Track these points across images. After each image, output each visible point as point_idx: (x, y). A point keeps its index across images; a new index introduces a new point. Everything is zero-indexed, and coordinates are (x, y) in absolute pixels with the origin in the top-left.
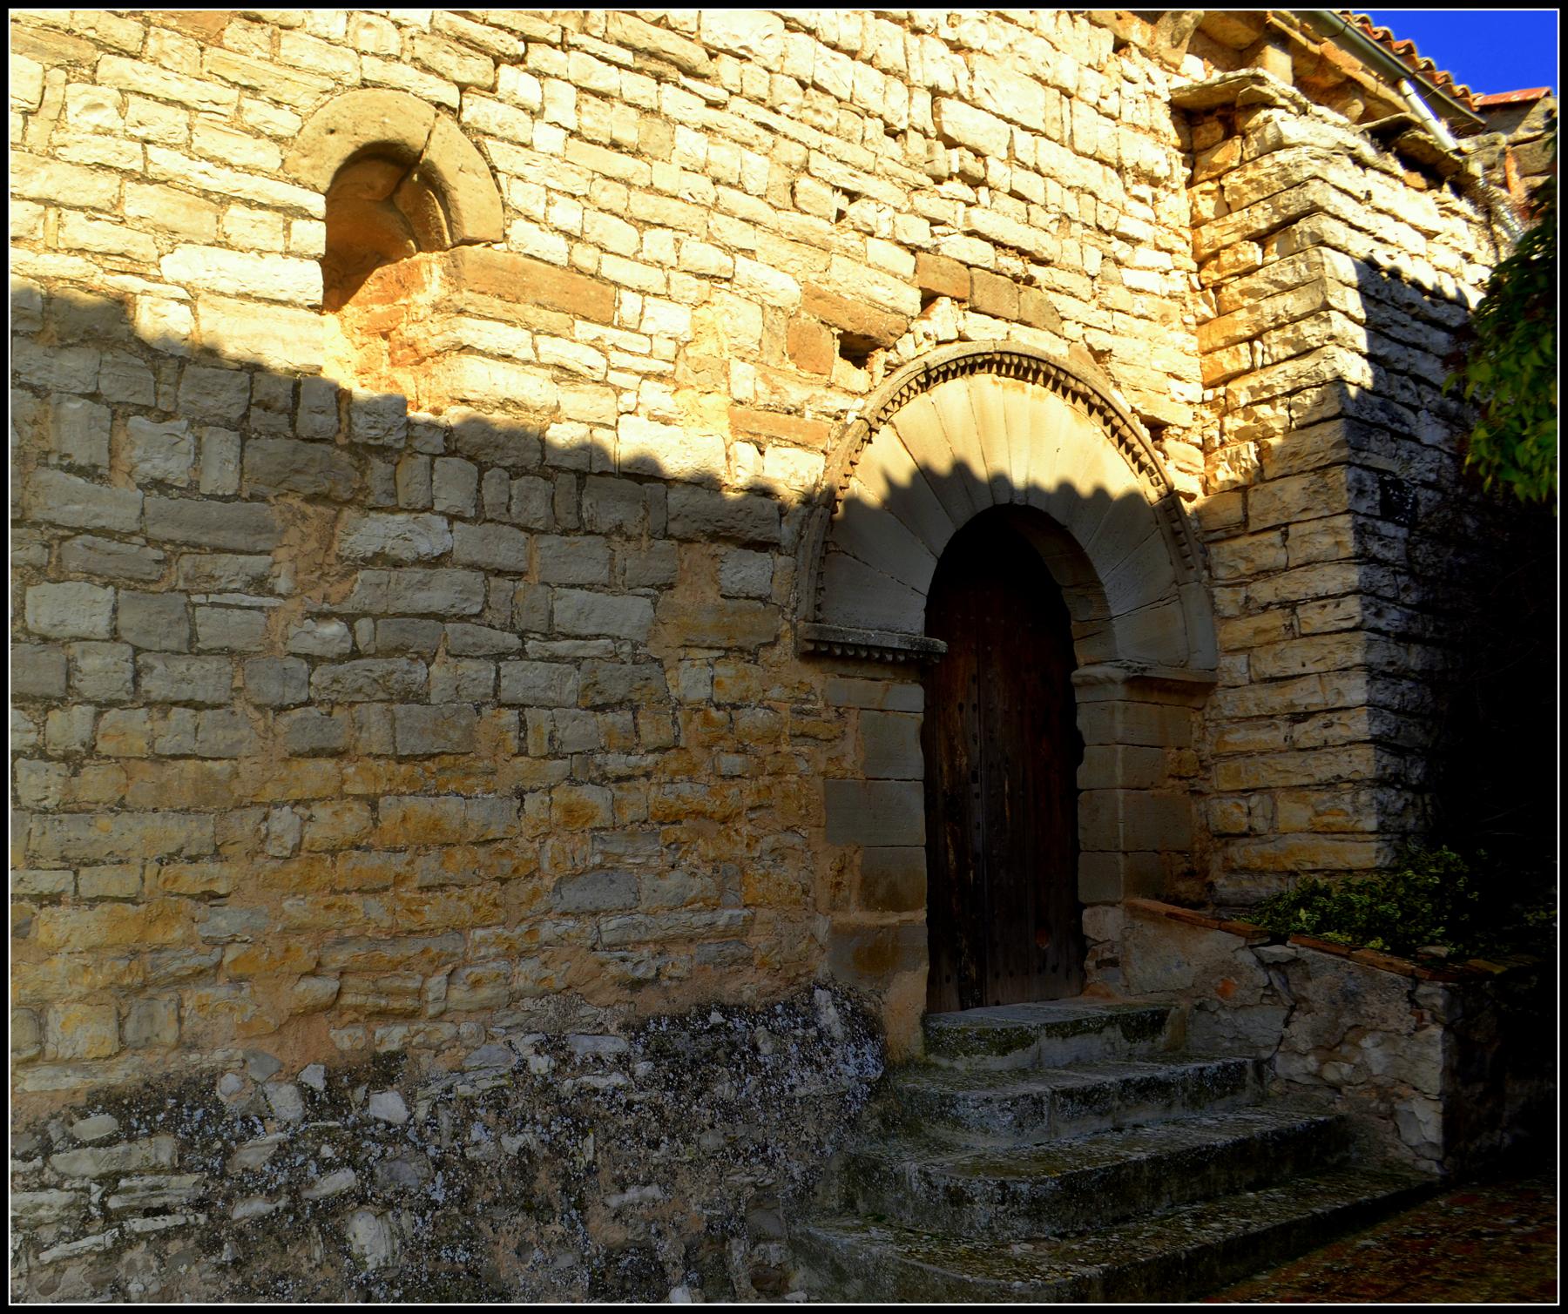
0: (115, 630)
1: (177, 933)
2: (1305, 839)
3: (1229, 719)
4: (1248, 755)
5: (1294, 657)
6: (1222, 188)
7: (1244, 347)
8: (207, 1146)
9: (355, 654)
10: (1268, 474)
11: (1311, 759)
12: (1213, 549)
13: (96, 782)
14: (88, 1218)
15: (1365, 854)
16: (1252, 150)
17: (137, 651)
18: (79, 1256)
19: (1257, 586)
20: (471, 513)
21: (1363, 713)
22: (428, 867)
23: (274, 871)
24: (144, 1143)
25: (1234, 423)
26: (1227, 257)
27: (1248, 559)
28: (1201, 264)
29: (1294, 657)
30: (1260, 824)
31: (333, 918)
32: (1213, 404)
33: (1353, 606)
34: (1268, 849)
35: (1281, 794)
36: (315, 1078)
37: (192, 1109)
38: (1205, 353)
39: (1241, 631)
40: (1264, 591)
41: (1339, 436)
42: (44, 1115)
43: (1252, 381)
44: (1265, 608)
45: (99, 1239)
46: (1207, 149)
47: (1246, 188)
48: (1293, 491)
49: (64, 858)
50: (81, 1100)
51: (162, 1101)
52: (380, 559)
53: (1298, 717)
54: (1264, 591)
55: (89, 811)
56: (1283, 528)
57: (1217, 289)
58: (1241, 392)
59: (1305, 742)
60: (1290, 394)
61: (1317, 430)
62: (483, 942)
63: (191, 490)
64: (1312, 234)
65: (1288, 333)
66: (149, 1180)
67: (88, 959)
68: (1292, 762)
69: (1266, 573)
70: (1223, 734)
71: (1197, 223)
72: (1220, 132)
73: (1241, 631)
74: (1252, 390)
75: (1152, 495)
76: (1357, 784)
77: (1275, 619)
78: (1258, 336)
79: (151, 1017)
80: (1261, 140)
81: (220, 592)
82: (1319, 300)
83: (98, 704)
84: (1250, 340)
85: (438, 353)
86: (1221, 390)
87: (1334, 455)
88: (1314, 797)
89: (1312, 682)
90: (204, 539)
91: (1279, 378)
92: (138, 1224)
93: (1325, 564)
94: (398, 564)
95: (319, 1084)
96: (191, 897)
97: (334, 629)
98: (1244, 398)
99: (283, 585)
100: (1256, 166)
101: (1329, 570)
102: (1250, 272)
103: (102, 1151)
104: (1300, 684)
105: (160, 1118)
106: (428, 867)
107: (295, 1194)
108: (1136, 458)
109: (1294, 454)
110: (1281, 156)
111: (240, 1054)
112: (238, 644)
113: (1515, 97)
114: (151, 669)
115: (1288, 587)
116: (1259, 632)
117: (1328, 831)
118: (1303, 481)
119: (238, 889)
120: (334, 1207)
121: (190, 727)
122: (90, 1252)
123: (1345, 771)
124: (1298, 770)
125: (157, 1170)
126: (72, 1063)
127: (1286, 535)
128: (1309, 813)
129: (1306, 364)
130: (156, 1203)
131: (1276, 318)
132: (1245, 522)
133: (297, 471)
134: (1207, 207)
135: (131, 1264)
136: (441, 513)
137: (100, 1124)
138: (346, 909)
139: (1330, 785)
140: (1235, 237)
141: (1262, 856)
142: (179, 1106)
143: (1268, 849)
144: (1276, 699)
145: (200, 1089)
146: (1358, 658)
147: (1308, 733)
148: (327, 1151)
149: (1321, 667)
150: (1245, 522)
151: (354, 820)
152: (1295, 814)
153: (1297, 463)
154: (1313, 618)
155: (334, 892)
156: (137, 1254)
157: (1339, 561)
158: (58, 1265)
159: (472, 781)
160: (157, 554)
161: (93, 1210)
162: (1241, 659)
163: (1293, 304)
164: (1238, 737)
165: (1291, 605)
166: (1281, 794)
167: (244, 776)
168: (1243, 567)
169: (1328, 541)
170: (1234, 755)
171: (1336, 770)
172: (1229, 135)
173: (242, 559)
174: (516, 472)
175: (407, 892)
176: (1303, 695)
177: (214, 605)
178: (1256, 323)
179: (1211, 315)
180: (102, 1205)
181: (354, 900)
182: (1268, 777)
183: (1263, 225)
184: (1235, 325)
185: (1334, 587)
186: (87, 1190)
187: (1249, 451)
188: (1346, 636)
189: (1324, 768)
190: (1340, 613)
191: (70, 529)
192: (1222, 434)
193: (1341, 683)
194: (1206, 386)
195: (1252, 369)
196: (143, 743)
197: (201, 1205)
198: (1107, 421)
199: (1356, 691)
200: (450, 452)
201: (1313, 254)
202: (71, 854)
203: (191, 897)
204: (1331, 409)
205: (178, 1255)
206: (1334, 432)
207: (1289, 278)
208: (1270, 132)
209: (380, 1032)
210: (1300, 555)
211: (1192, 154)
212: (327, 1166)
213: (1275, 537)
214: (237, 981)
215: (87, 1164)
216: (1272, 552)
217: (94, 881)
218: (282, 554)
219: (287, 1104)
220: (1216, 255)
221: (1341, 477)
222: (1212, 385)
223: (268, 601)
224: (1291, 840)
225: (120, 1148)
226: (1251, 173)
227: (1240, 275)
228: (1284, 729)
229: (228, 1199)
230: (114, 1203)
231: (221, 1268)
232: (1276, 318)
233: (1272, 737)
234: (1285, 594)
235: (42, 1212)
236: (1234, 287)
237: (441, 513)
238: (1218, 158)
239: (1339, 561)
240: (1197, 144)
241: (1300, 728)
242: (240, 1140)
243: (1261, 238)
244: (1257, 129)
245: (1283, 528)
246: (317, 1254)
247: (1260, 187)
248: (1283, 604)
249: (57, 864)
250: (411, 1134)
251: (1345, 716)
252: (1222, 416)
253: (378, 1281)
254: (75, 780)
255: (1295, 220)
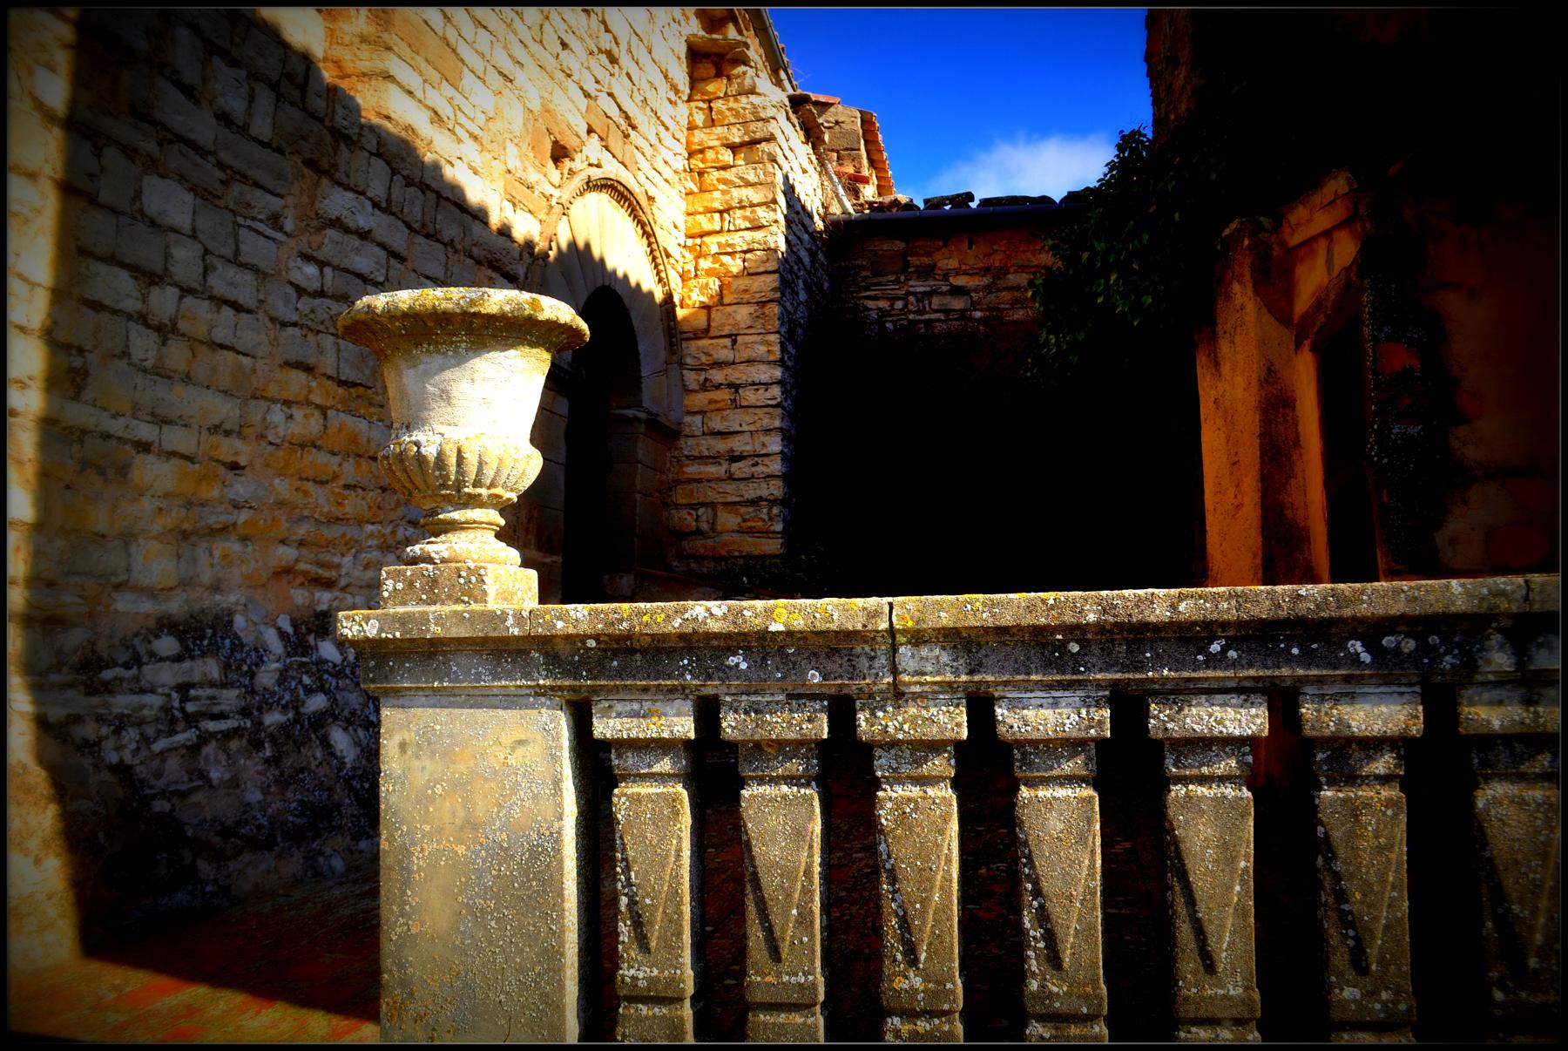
0: (194, 230)
1: (215, 493)
2: (736, 536)
3: (688, 457)
4: (700, 481)
5: (735, 421)
6: (711, 109)
7: (717, 216)
8: (239, 668)
9: (321, 294)
10: (727, 300)
11: (742, 485)
12: (684, 345)
13: (177, 356)
14: (173, 720)
15: (773, 546)
16: (733, 89)
17: (206, 251)
18: (176, 749)
19: (713, 372)
20: (384, 205)
21: (778, 459)
22: (350, 472)
23: (271, 454)
24: (199, 662)
25: (705, 264)
26: (710, 155)
27: (707, 354)
28: (691, 155)
29: (735, 421)
30: (705, 526)
31: (298, 499)
32: (691, 249)
33: (776, 391)
34: (710, 542)
35: (720, 508)
36: (285, 623)
37: (223, 638)
38: (689, 214)
39: (700, 399)
40: (718, 376)
41: (776, 284)
42: (129, 633)
43: (721, 239)
44: (718, 387)
45: (186, 735)
46: (703, 80)
47: (728, 113)
48: (743, 314)
49: (152, 414)
50: (152, 623)
51: (203, 630)
52: (337, 223)
53: (734, 458)
54: (718, 376)
55: (169, 378)
56: (733, 337)
57: (701, 174)
58: (712, 244)
59: (738, 475)
60: (745, 252)
61: (762, 278)
62: (371, 536)
63: (244, 130)
64: (769, 154)
65: (748, 212)
66: (209, 692)
67: (163, 504)
68: (730, 487)
69: (720, 365)
70: (682, 466)
71: (691, 127)
72: (713, 72)
73: (700, 399)
74: (719, 245)
75: (659, 296)
76: (772, 502)
77: (724, 395)
78: (727, 211)
79: (195, 560)
80: (741, 85)
81: (253, 219)
82: (770, 196)
83: (182, 289)
84: (721, 212)
85: (364, 75)
86: (698, 241)
87: (771, 296)
88: (742, 510)
89: (747, 437)
90: (249, 173)
91: (740, 240)
92: (212, 726)
93: (760, 365)
94: (347, 230)
95: (290, 630)
96: (224, 464)
97: (311, 269)
98: (714, 249)
99: (289, 225)
100: (736, 100)
101: (763, 367)
102: (725, 168)
103: (176, 666)
104: (738, 438)
105: (206, 642)
106: (350, 472)
107: (296, 708)
108: (658, 274)
109: (745, 291)
110: (753, 98)
111: (243, 600)
112: (262, 265)
113: (822, 99)
114: (215, 268)
115: (736, 375)
116: (711, 402)
117: (751, 531)
118: (751, 309)
119: (251, 463)
120: (319, 722)
121: (232, 324)
122: (183, 746)
123: (764, 493)
124: (732, 492)
125: (212, 685)
126: (151, 593)
127: (734, 342)
128: (739, 520)
129: (758, 235)
130: (216, 709)
131: (741, 201)
132: (708, 330)
133: (303, 138)
134: (699, 118)
135: (207, 759)
136: (370, 199)
137: (167, 645)
138: (306, 493)
139: (755, 502)
140: (717, 143)
141: (705, 547)
142: (214, 635)
143: (710, 542)
144: (721, 446)
145: (223, 622)
146: (777, 423)
147: (740, 469)
148: (306, 680)
149: (752, 428)
150: (708, 330)
151: (314, 425)
152: (728, 520)
153: (746, 297)
154: (750, 396)
155: (301, 479)
156: (210, 749)
157: (769, 363)
158: (163, 755)
159: (372, 410)
160: (220, 175)
161: (177, 713)
162: (698, 419)
163: (754, 195)
164: (692, 470)
165: (735, 387)
166: (720, 508)
167: (259, 372)
168: (704, 359)
169: (763, 349)
170: (690, 481)
171: (759, 493)
172: (719, 75)
173: (269, 197)
174: (409, 182)
175: (336, 487)
176: (739, 445)
177: (250, 228)
178: (727, 202)
179: (696, 190)
180: (182, 709)
181: (310, 486)
182: (713, 496)
183: (737, 140)
184: (713, 200)
185: (764, 378)
186: (169, 696)
187: (714, 284)
188: (770, 410)
189: (751, 492)
190: (768, 395)
191: (175, 135)
192: (696, 269)
193: (766, 439)
194: (689, 236)
195: (721, 231)
196: (204, 329)
197: (245, 712)
198: (649, 245)
199: (775, 444)
200: (379, 155)
201: (769, 166)
202: (158, 411)
203: (224, 464)
204: (772, 266)
205: (238, 751)
206: (772, 281)
207: (752, 178)
208: (748, 82)
209: (317, 595)
210: (745, 354)
211: (694, 81)
212: (309, 691)
213: (727, 342)
214: (244, 539)
215: (167, 675)
216: (725, 351)
217: (176, 439)
218: (290, 200)
219: (277, 646)
220: (702, 151)
221: (775, 309)
222: (692, 237)
223: (279, 236)
224: (726, 537)
225: (187, 664)
226: (732, 104)
227: (718, 169)
228: (725, 466)
229: (260, 709)
230: (191, 707)
231: (267, 761)
232: (741, 201)
233: (713, 470)
234: (732, 379)
235: (146, 712)
236: (714, 175)
237: (370, 199)
238: (711, 88)
239: (769, 363)
240: (696, 75)
241: (735, 466)
242: (257, 665)
243: (734, 148)
244: (738, 76)
245: (733, 337)
246: (318, 755)
247: (737, 115)
248: (731, 386)
249: (149, 418)
250: (348, 671)
251: (766, 461)
252: (697, 258)
253: (354, 777)
254: (164, 349)
255: (759, 142)
